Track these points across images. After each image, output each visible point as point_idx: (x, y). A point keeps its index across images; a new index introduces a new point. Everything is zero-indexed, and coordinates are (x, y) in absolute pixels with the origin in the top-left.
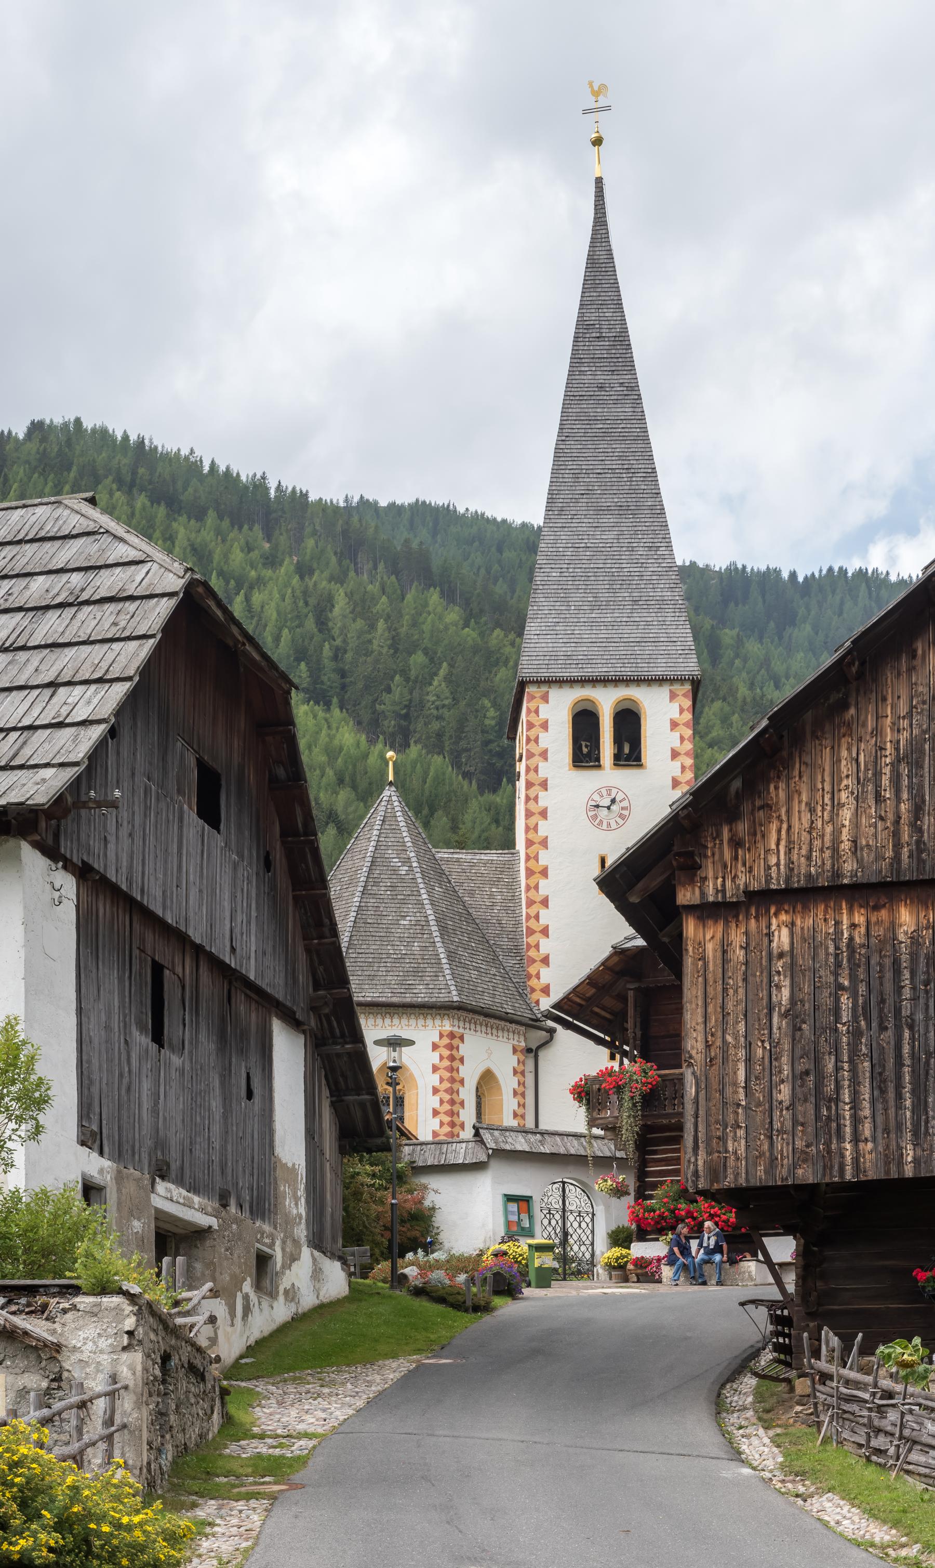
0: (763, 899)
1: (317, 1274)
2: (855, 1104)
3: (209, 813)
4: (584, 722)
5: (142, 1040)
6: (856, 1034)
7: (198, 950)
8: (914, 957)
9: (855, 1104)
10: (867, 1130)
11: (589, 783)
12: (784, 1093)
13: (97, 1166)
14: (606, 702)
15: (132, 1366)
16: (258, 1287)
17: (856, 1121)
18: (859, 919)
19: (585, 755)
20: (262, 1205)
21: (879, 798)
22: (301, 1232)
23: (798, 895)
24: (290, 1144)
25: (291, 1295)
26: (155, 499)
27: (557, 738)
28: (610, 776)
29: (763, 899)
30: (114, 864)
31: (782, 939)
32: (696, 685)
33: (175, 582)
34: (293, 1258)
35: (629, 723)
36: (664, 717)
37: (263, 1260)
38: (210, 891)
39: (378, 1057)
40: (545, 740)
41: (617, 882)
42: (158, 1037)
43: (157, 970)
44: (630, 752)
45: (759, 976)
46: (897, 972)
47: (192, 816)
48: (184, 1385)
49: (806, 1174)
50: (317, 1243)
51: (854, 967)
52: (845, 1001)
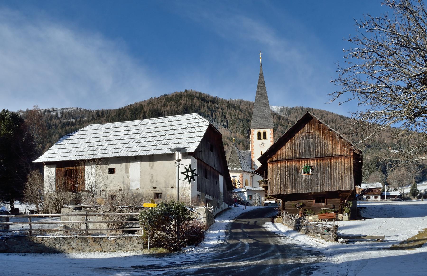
0: (276, 161)
1: (225, 205)
2: (288, 185)
3: (212, 151)
4: (259, 134)
5: (204, 178)
6: (288, 177)
7: (211, 167)
8: (295, 168)
9: (288, 185)
10: (289, 188)
11: (260, 141)
12: (279, 184)
13: (199, 193)
14: (262, 131)
15: (205, 215)
16: (218, 207)
17: (288, 187)
18: (288, 163)
19: (259, 138)
20: (218, 197)
21: (291, 149)
22: (223, 200)
23: (281, 160)
24: (221, 190)
25: (222, 208)
26: (202, 100)
27: (256, 136)
28: (262, 141)
29: (276, 161)
30: (202, 157)
31: (279, 166)
32: (274, 129)
33: (208, 124)
34: (222, 203)
35: (265, 134)
36: (269, 132)
37: (218, 204)
38: (213, 162)
39: (232, 178)
40: (254, 136)
41: (260, 159)
42: (206, 178)
43: (206, 169)
44: (265, 137)
45: (277, 170)
46: (293, 169)
47: (210, 152)
48: (210, 218)
49: (282, 193)
50: (225, 202)
51: (288, 169)
52: (287, 173)
